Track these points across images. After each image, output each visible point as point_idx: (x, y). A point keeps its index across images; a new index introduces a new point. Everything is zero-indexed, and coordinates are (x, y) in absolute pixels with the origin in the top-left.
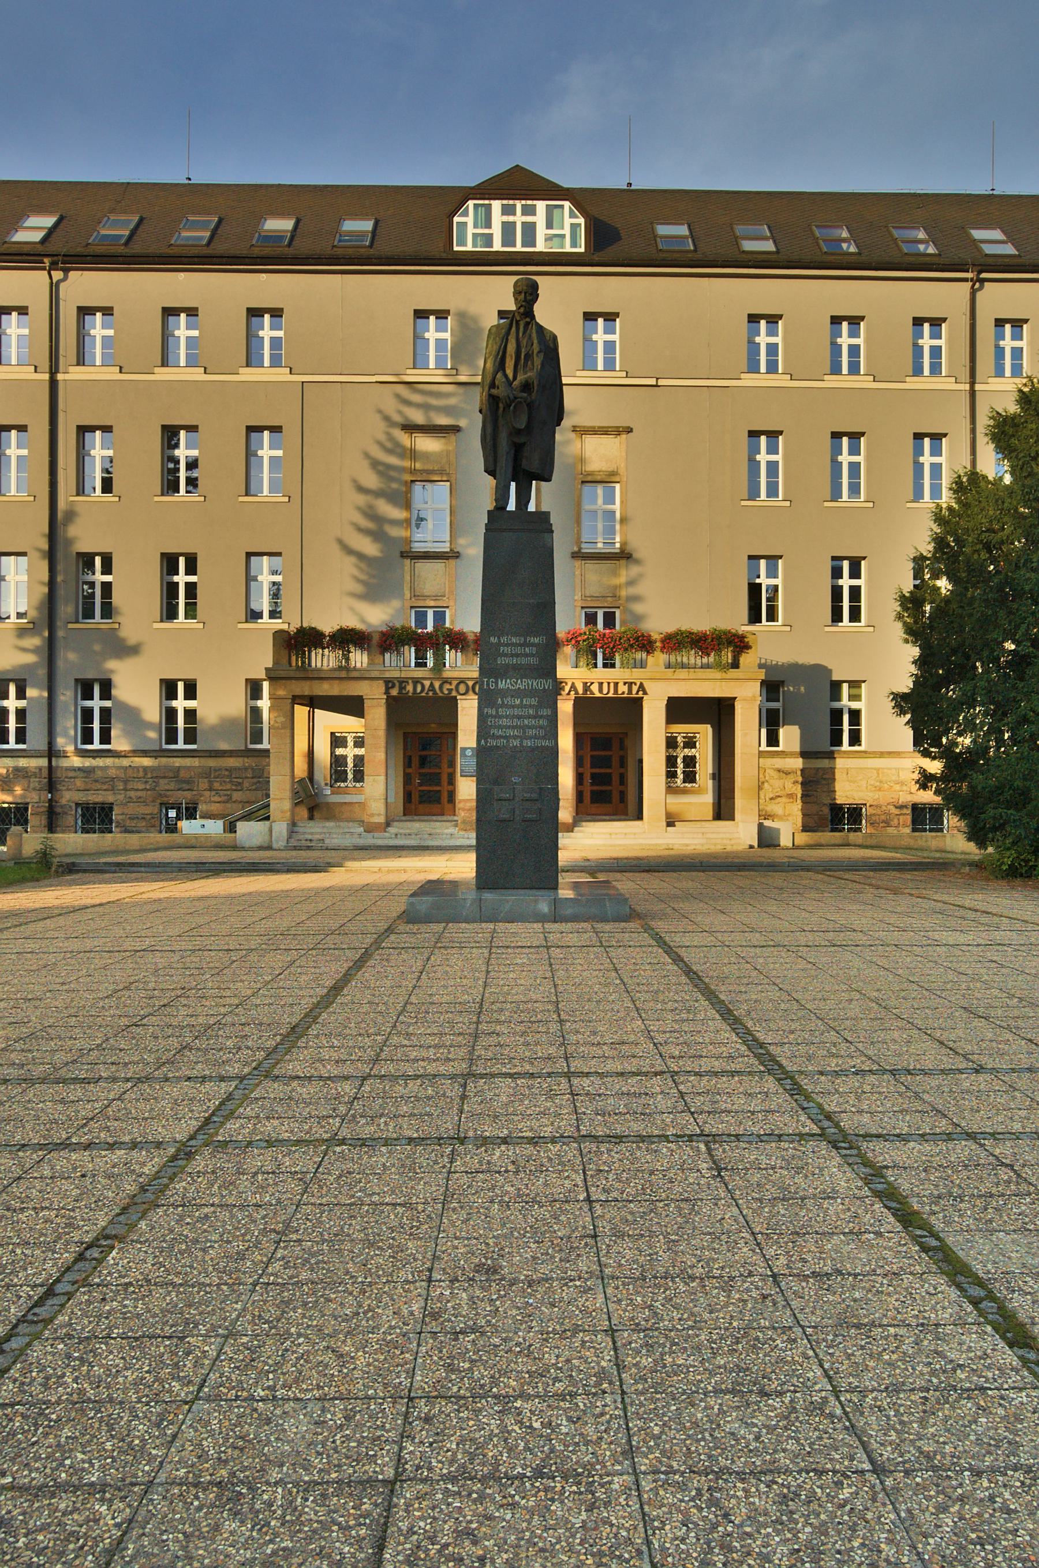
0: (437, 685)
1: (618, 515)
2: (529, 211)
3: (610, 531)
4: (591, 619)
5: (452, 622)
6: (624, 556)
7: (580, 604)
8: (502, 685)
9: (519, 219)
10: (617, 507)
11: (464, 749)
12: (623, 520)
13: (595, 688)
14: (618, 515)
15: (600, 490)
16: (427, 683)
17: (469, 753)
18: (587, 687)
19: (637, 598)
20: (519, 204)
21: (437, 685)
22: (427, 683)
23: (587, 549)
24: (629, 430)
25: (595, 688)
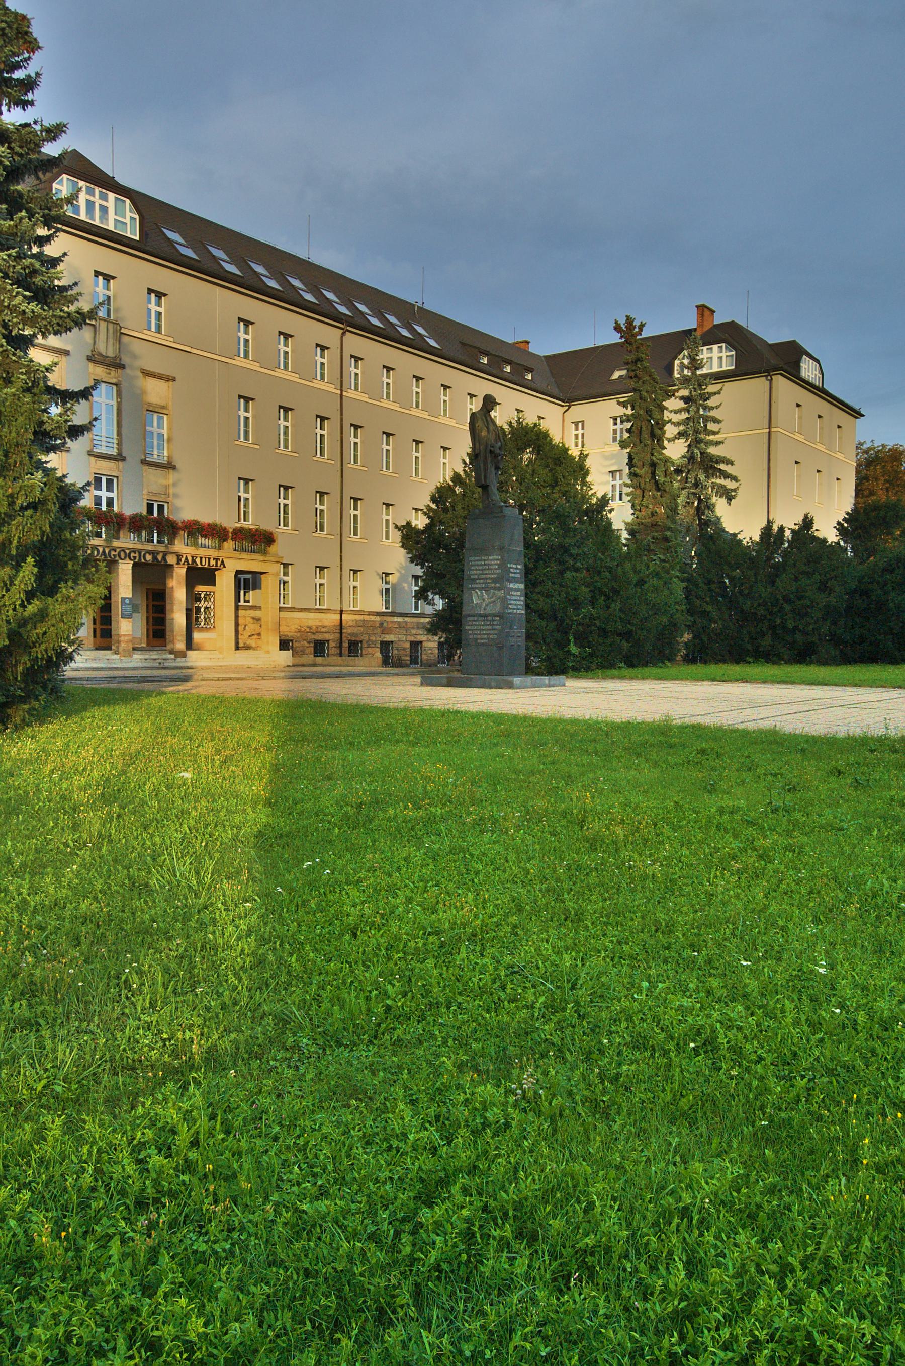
0: (107, 551)
1: (166, 437)
2: (104, 197)
3: (160, 447)
4: (150, 507)
5: (120, 505)
6: (169, 466)
7: (146, 497)
8: (512, 586)
9: (98, 202)
10: (165, 432)
11: (123, 599)
12: (169, 440)
13: (198, 561)
14: (166, 437)
15: (155, 416)
16: (101, 549)
17: (127, 601)
18: (194, 561)
19: (176, 496)
20: (97, 190)
21: (107, 551)
22: (101, 549)
23: (155, 458)
24: (174, 380)
25: (198, 561)
